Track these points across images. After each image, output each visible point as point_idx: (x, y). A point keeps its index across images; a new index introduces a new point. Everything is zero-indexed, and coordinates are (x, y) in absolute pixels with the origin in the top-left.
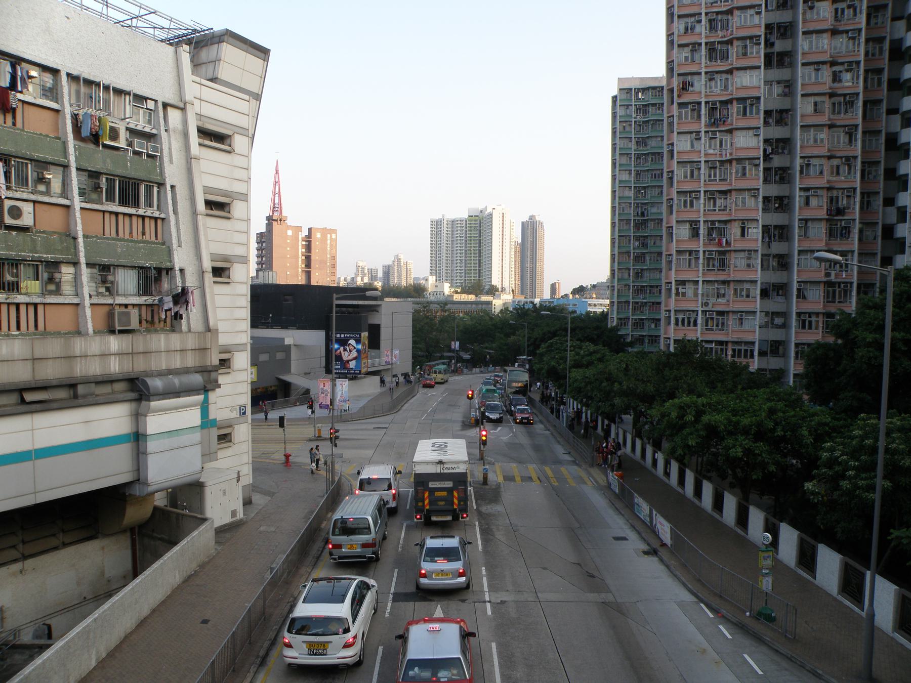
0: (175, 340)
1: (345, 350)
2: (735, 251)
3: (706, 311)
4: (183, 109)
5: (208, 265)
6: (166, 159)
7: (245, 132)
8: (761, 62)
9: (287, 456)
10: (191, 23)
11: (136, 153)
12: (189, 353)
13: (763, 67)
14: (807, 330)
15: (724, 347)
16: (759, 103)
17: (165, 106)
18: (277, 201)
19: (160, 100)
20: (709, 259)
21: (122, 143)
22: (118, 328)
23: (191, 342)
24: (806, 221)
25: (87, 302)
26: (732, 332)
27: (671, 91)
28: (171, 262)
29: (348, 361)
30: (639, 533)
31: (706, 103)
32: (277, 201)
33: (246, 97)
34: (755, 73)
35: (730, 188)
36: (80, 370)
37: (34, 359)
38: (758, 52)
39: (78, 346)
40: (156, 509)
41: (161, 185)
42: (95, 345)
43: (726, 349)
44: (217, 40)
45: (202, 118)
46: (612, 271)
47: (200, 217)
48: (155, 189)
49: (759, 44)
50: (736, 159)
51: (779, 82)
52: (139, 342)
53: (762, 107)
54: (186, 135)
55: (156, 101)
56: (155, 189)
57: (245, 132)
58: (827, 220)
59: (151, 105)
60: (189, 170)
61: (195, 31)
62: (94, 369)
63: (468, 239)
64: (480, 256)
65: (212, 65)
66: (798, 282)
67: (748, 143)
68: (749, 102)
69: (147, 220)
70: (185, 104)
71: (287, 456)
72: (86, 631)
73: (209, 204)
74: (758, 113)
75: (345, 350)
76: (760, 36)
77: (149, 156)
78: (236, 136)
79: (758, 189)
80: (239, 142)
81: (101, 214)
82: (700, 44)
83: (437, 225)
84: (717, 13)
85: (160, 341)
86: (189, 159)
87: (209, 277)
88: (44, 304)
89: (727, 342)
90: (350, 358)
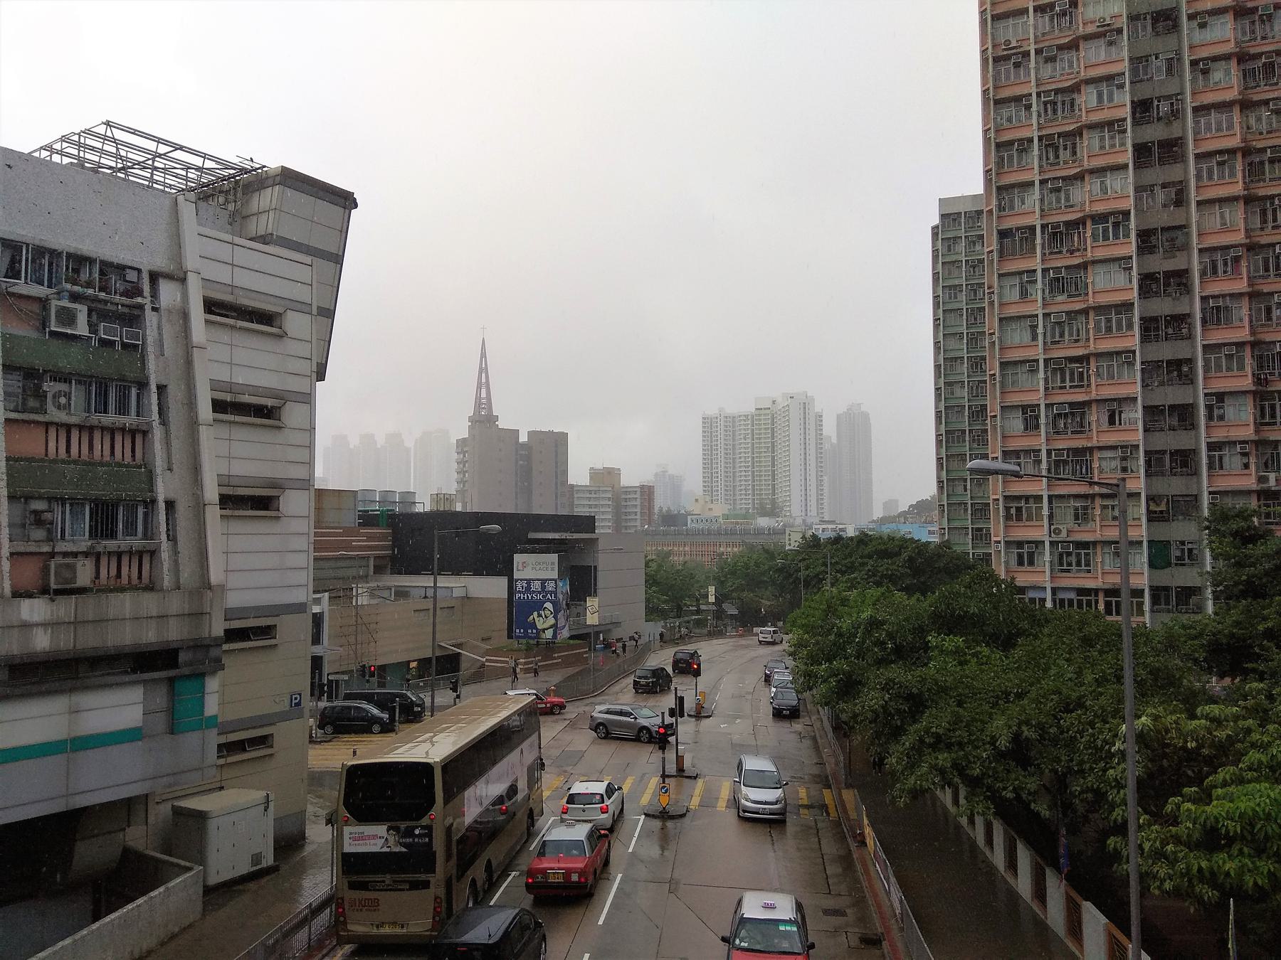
0: (149, 603)
2: (1100, 448)
3: (1057, 542)
4: (183, 280)
5: (211, 492)
6: (151, 349)
7: (307, 309)
8: (1128, 157)
10: (236, 160)
11: (105, 343)
12: (172, 621)
13: (1131, 166)
14: (1026, 568)
15: (1093, 598)
16: (1128, 219)
17: (154, 277)
18: (484, 395)
20: (1057, 463)
21: (82, 328)
22: (53, 586)
23: (176, 604)
24: (1221, 396)
26: (1102, 574)
27: (990, 211)
28: (152, 491)
29: (544, 630)
30: (871, 886)
31: (1044, 227)
32: (484, 395)
33: (308, 259)
34: (1119, 175)
35: (1087, 352)
38: (1123, 144)
40: (127, 853)
41: (143, 385)
43: (1097, 602)
44: (270, 182)
45: (236, 291)
46: (940, 482)
47: (202, 429)
48: (134, 392)
49: (1125, 131)
50: (1094, 308)
51: (1164, 186)
52: (89, 607)
53: (1133, 225)
54: (185, 316)
55: (139, 271)
56: (134, 392)
57: (307, 309)
58: (1254, 393)
59: (132, 276)
60: (189, 363)
61: (243, 171)
63: (749, 441)
64: (773, 465)
65: (255, 218)
66: (1210, 493)
67: (1114, 285)
68: (1111, 219)
69: (97, 435)
70: (185, 273)
73: (219, 406)
74: (1127, 236)
75: (539, 615)
76: (1125, 120)
77: (125, 346)
78: (291, 315)
79: (1134, 352)
80: (295, 323)
81: (42, 430)
82: (1031, 140)
83: (709, 424)
84: (1057, 91)
85: (124, 604)
86: (188, 347)
87: (213, 513)
89: (1096, 591)
90: (545, 626)
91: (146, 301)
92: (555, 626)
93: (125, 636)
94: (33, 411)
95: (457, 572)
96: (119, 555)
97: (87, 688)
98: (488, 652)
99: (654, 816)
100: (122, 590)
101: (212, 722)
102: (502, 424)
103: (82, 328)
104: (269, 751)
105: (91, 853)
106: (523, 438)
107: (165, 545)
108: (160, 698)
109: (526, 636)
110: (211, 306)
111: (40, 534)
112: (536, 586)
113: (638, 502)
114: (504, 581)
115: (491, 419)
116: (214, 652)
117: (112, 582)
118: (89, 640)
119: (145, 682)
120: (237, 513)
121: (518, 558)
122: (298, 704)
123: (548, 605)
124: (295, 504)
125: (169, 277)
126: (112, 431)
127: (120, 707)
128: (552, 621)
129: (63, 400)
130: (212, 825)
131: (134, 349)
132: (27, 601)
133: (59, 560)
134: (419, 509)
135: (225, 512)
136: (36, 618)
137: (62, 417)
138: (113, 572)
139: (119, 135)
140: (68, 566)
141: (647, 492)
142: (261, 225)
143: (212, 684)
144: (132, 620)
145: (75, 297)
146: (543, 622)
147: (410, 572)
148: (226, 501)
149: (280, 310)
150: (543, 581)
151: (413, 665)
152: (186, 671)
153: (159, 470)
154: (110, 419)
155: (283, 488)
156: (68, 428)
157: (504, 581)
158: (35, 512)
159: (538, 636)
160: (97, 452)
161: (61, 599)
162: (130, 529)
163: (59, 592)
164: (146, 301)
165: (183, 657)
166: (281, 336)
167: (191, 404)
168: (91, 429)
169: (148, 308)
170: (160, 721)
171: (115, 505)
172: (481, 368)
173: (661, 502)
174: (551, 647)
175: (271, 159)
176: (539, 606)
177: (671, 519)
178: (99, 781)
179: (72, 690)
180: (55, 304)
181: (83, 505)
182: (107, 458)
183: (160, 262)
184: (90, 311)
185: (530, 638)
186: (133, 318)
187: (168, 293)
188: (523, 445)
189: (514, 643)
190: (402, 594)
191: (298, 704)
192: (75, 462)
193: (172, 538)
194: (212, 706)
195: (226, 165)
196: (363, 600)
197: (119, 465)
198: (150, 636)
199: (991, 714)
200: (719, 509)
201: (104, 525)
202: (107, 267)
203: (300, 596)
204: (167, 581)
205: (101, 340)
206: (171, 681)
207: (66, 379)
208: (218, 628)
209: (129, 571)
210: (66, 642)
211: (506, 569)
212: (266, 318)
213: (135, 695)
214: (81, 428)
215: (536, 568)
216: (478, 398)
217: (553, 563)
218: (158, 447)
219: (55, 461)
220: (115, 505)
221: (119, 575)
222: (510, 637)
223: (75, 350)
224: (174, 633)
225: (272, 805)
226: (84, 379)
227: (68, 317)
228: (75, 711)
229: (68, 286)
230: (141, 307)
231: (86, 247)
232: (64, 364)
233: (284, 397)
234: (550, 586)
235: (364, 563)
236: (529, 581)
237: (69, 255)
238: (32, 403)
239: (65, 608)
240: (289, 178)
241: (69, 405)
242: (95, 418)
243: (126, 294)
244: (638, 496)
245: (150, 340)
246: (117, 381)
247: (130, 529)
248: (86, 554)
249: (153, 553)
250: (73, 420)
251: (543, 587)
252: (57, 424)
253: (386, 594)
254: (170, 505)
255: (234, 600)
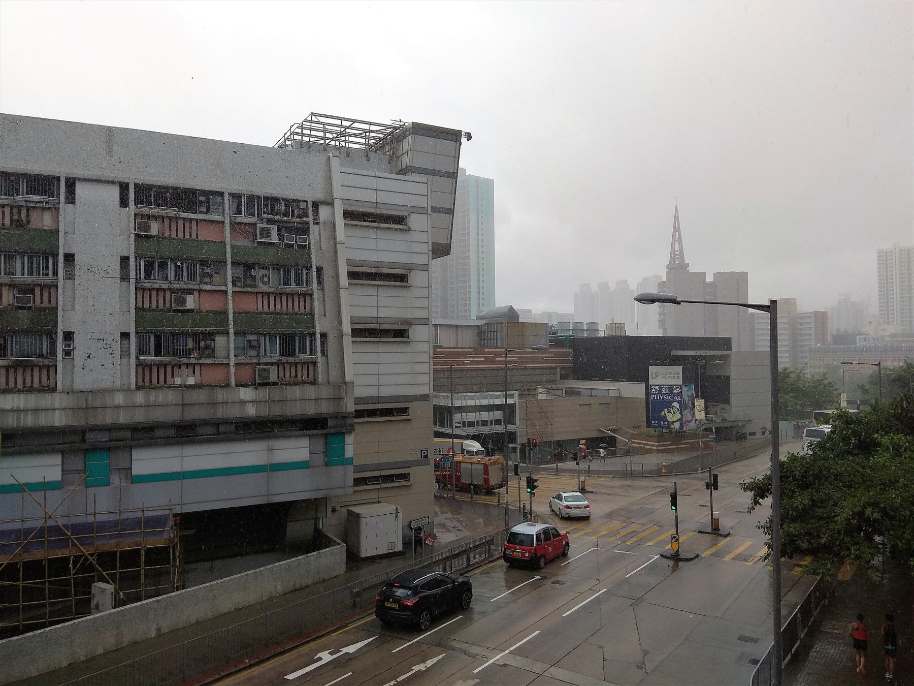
1: (669, 412)
5: (347, 328)
9: (674, 502)
17: (316, 205)
18: (677, 248)
19: (310, 200)
21: (274, 238)
23: (325, 392)
25: (232, 363)
32: (677, 248)
36: (221, 413)
37: (183, 405)
39: (221, 395)
42: (246, 394)
47: (342, 291)
52: (276, 393)
56: (305, 272)
59: (302, 205)
61: (395, 128)
62: (234, 413)
71: (674, 502)
72: (35, 636)
73: (352, 275)
87: (348, 340)
88: (200, 364)
90: (674, 419)
91: (310, 219)
92: (680, 420)
93: (296, 410)
94: (250, 286)
95: (615, 379)
96: (296, 364)
97: (276, 437)
98: (633, 436)
99: (666, 557)
100: (295, 384)
101: (350, 461)
102: (691, 269)
103: (274, 238)
104: (407, 483)
105: (297, 529)
106: (710, 279)
107: (320, 359)
108: (320, 445)
109: (660, 426)
110: (348, 215)
111: (253, 353)
112: (666, 390)
113: (812, 325)
114: (643, 385)
115: (683, 266)
116: (349, 421)
117: (293, 379)
118: (277, 411)
119: (310, 436)
120: (383, 339)
121: (652, 369)
122: (426, 456)
123: (676, 404)
124: (418, 333)
125: (324, 203)
126: (292, 295)
127: (295, 449)
128: (678, 416)
129: (266, 279)
130: (363, 522)
131: (304, 248)
132: (243, 389)
133: (262, 367)
134: (601, 334)
135: (355, 339)
136: (248, 398)
137: (265, 288)
138: (293, 374)
139: (322, 120)
140: (265, 370)
141: (821, 318)
142: (405, 162)
143: (349, 439)
144: (301, 401)
145: (269, 221)
146: (672, 416)
147: (585, 378)
148: (356, 333)
149: (404, 214)
150: (671, 387)
151: (583, 442)
152: (332, 431)
153: (316, 316)
154: (293, 287)
155: (411, 324)
156: (268, 294)
157: (643, 385)
158: (250, 341)
159: (668, 427)
160: (272, 306)
161: (261, 389)
162: (303, 350)
163: (260, 384)
164: (310, 219)
165: (331, 423)
166: (408, 230)
167: (337, 277)
168: (281, 294)
169: (311, 223)
170: (319, 459)
171: (293, 337)
172: (674, 227)
173: (835, 325)
174: (679, 436)
175: (409, 119)
176: (668, 405)
177: (842, 338)
178: (291, 488)
179: (268, 438)
180: (258, 225)
181: (276, 337)
182: (290, 310)
183: (319, 195)
184: (279, 230)
185: (663, 428)
186: (304, 230)
187: (324, 211)
188: (711, 285)
189: (652, 430)
190: (571, 392)
191: (426, 456)
192: (272, 313)
193: (323, 353)
194: (349, 452)
195: (388, 127)
196: (543, 396)
197: (297, 314)
198: (311, 410)
199: (794, 492)
200: (891, 329)
201: (287, 347)
202: (289, 202)
203: (425, 390)
204: (321, 378)
205: (286, 245)
206: (326, 435)
207: (263, 267)
208: (351, 407)
209: (302, 374)
210: (264, 412)
211: (644, 377)
212: (400, 220)
213: (305, 442)
214: (275, 294)
215: (665, 377)
216: (673, 251)
217: (678, 373)
218: (316, 303)
219: (261, 313)
220: (293, 337)
221: (296, 376)
222: (648, 426)
223: (272, 250)
224: (325, 408)
225: (400, 515)
226: (276, 267)
227: (266, 233)
228: (271, 450)
229: (265, 216)
230: (308, 223)
231: (276, 192)
232: (263, 260)
233: (410, 268)
234: (677, 390)
235: (553, 371)
236: (660, 387)
237: (266, 198)
238: (249, 282)
239: (263, 393)
240: (419, 129)
241: (270, 282)
242: (282, 288)
243: (299, 216)
244: (812, 320)
245: (312, 242)
246: (295, 265)
247: (303, 350)
248: (278, 364)
249: (315, 363)
250: (270, 290)
251: (671, 391)
252: (262, 293)
253: (559, 393)
254: (324, 336)
255: (359, 392)
